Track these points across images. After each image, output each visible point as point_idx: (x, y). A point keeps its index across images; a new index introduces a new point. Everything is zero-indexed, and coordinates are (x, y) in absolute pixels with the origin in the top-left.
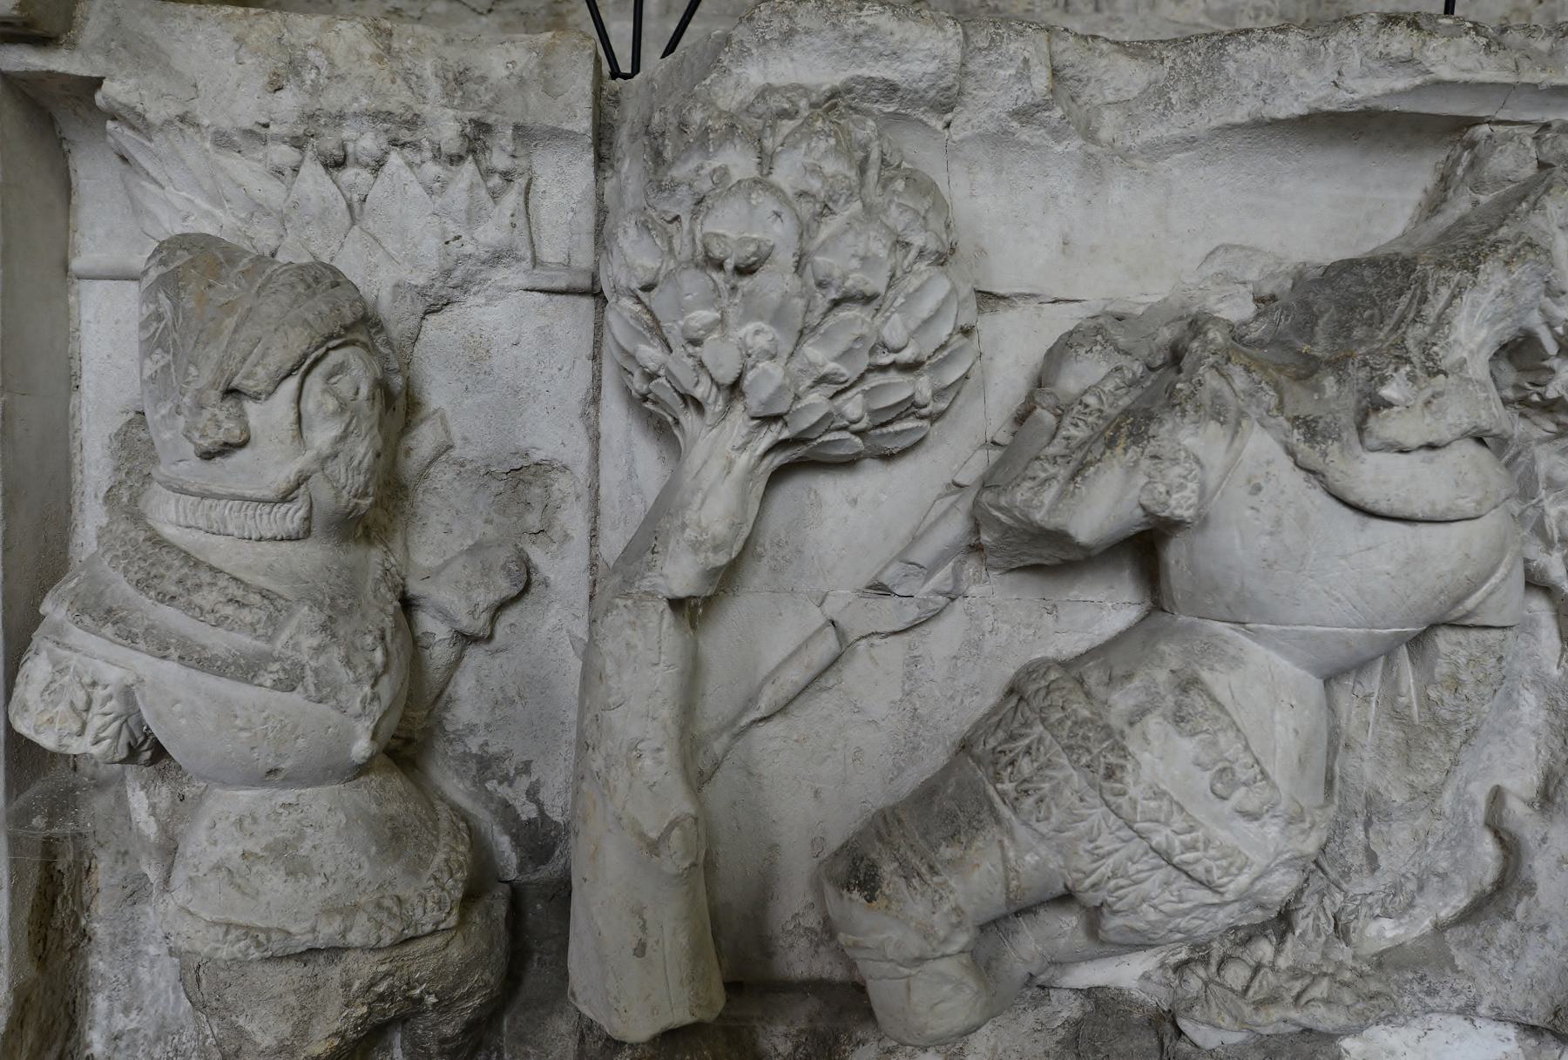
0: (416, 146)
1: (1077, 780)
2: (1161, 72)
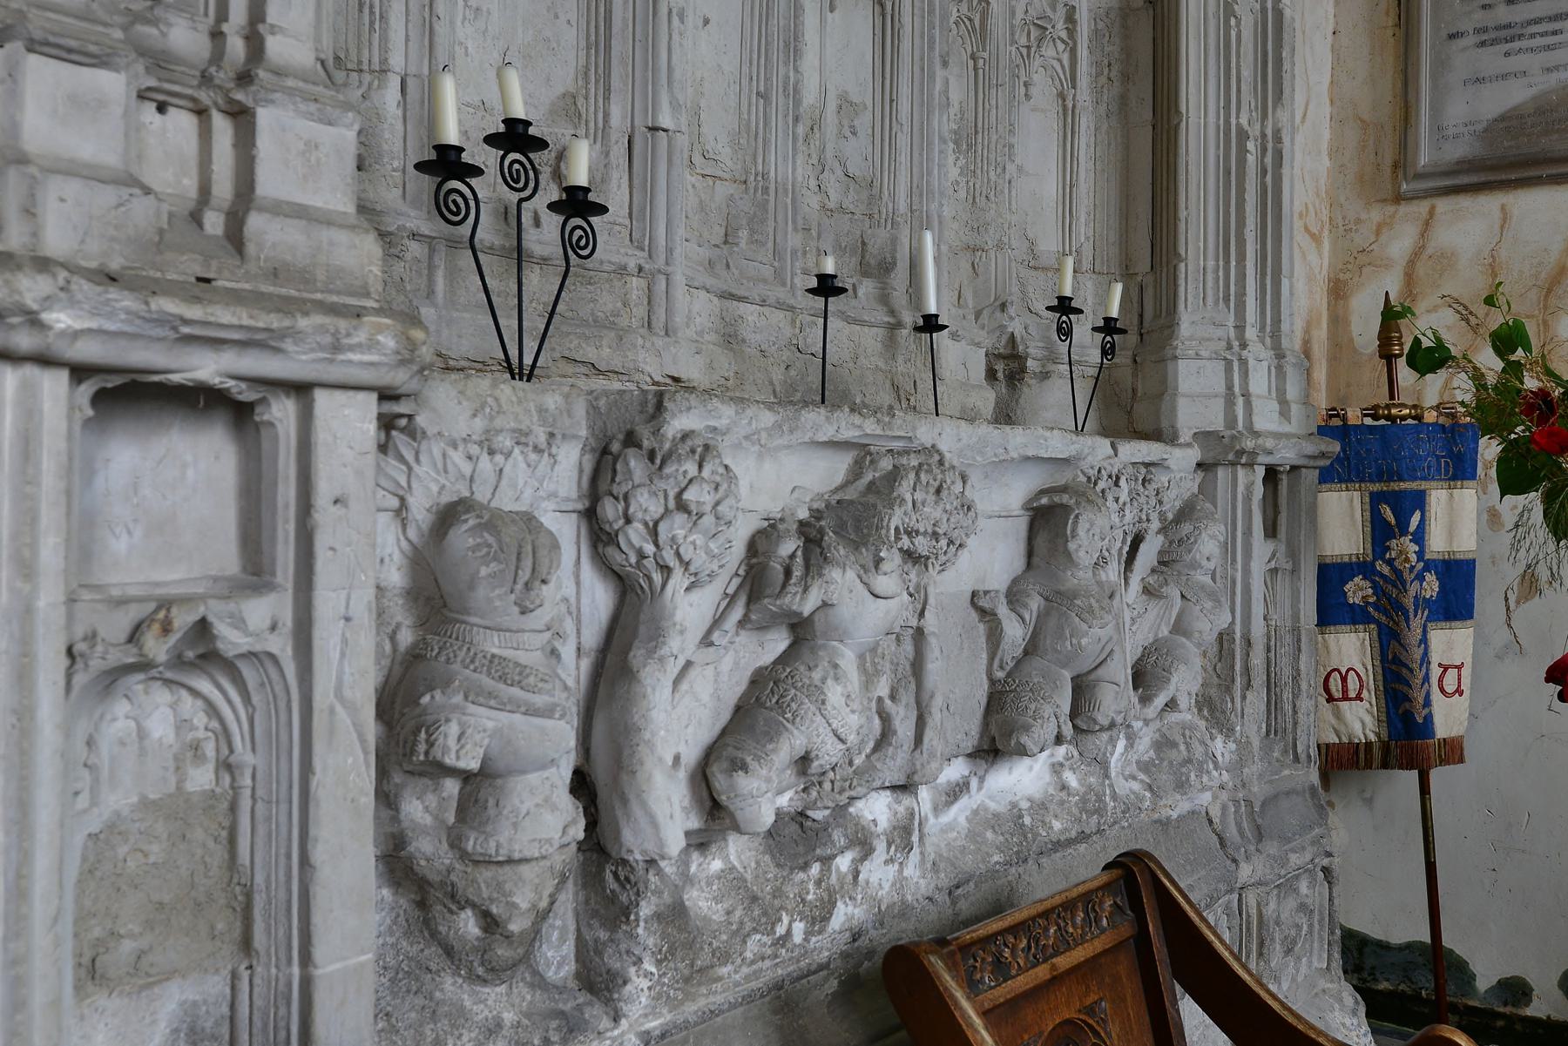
0: (526, 445)
1: (813, 708)
2: (779, 417)
